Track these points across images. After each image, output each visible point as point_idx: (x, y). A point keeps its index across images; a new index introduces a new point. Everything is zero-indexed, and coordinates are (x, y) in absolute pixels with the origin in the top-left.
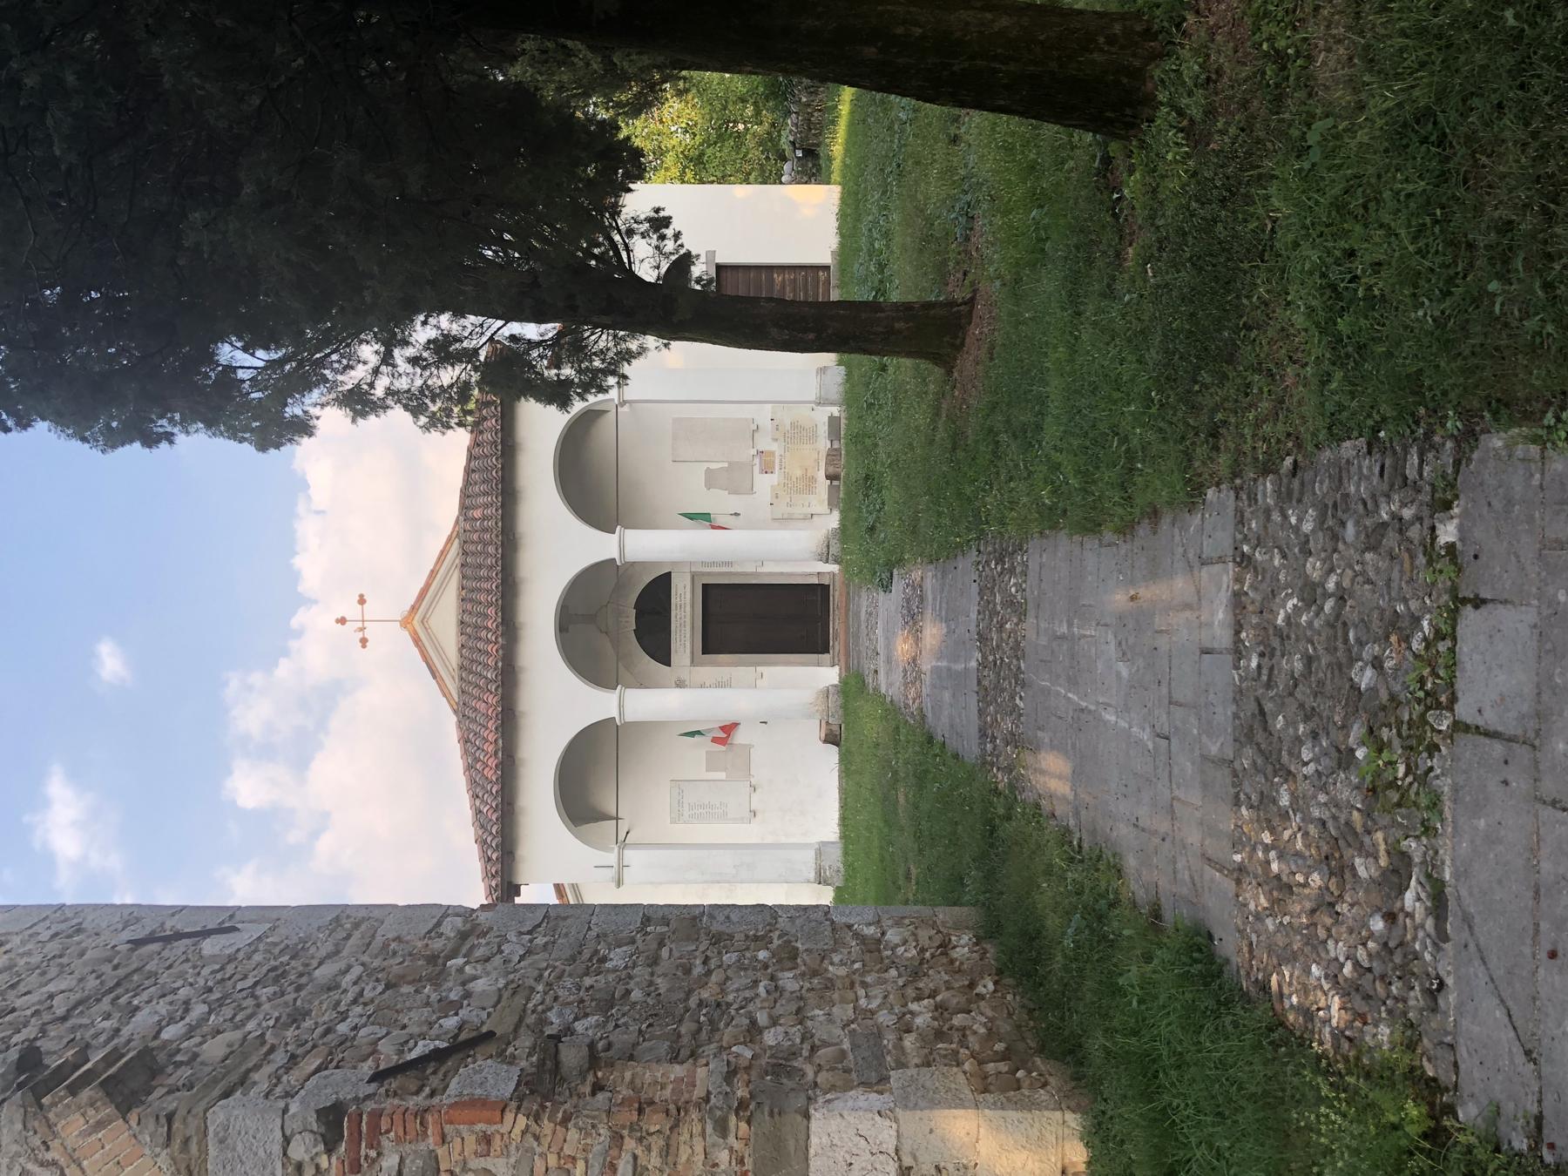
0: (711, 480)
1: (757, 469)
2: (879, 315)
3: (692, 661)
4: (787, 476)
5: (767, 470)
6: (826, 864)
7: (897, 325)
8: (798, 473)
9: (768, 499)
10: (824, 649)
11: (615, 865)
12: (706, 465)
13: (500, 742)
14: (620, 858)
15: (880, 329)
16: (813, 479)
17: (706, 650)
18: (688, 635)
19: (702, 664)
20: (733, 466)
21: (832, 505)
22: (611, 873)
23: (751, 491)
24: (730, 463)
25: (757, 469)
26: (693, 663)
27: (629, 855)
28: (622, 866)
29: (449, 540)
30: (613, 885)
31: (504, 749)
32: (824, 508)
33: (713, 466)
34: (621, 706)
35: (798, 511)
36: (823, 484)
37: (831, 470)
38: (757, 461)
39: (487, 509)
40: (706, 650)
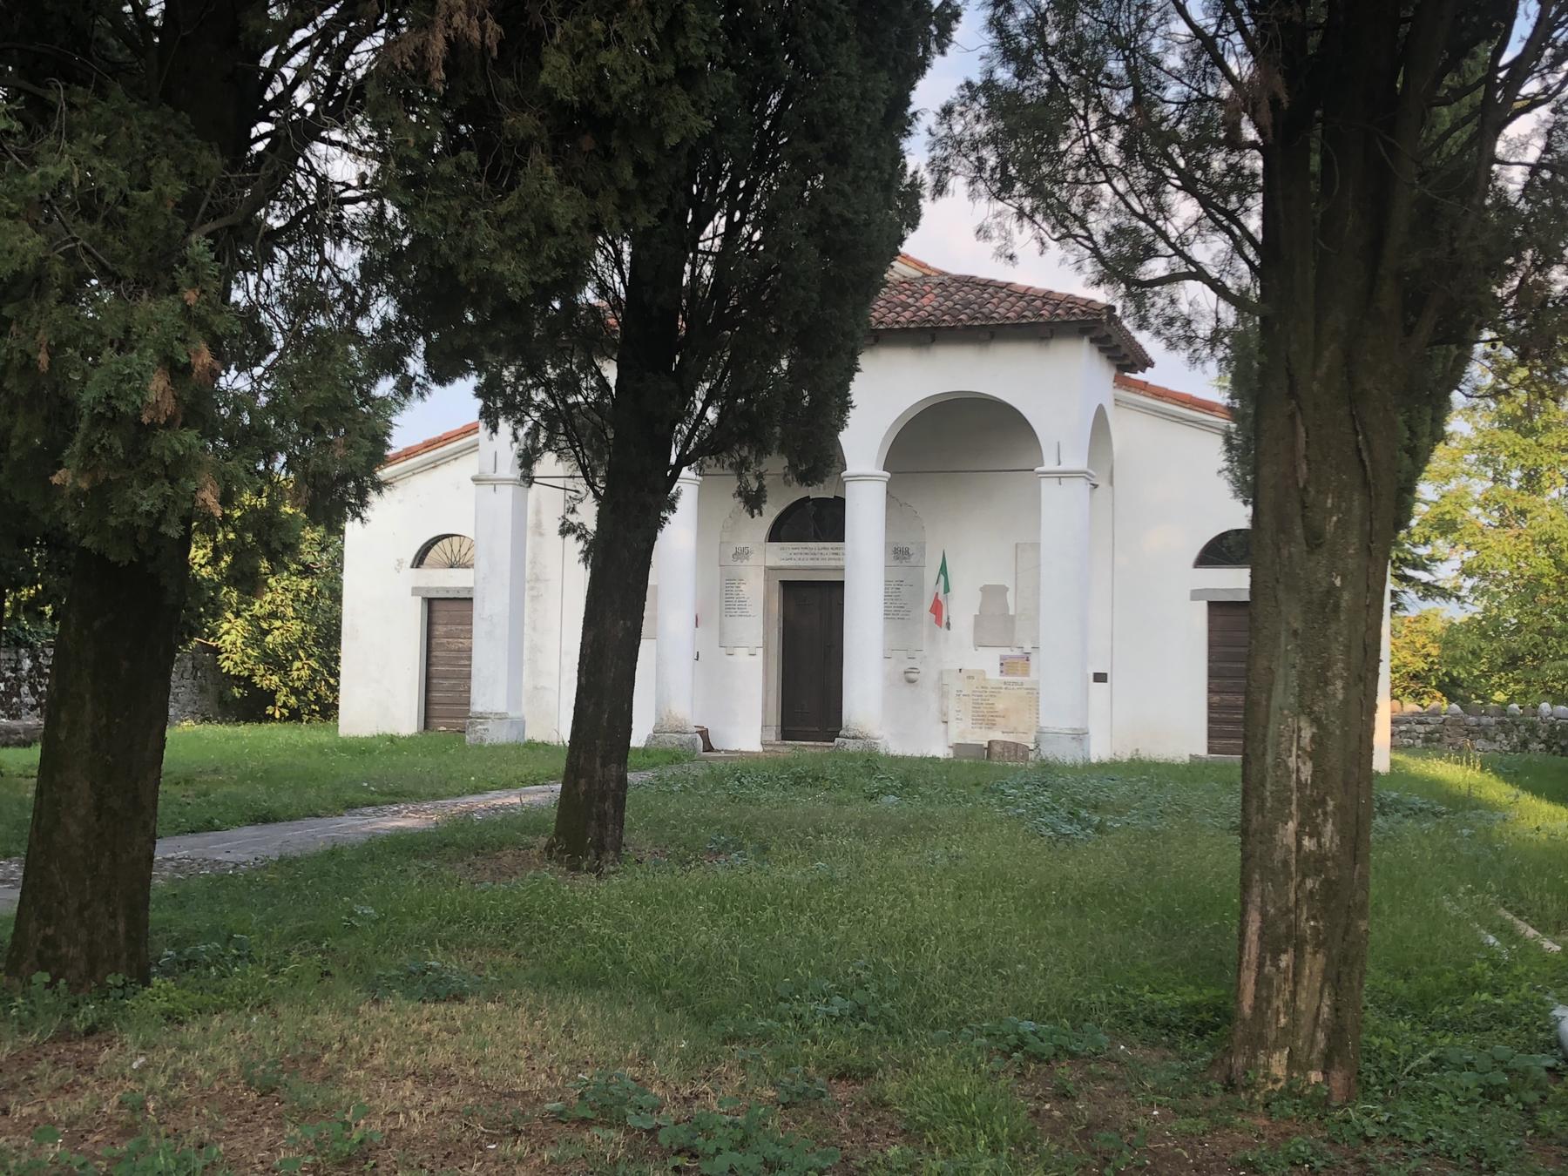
0: (992, 593)
1: (1007, 652)
2: (598, 761)
3: (772, 569)
4: (995, 691)
5: (1006, 666)
6: (490, 725)
7: (583, 781)
8: (1000, 706)
9: (969, 666)
10: (787, 733)
11: (496, 476)
12: (1010, 584)
13: (897, 326)
14: (504, 481)
15: (582, 761)
16: (991, 725)
17: (787, 586)
18: (801, 563)
19: (767, 580)
20: (1009, 621)
21: (958, 748)
22: (489, 472)
23: (979, 645)
24: (1013, 617)
25: (1007, 652)
26: (770, 570)
27: (507, 492)
28: (495, 483)
29: (920, 265)
30: (475, 473)
31: (890, 331)
32: (956, 739)
33: (1010, 597)
34: (1060, 476)
35: (952, 704)
36: (981, 737)
37: (997, 749)
38: (1017, 652)
39: (1003, 311)
40: (787, 586)
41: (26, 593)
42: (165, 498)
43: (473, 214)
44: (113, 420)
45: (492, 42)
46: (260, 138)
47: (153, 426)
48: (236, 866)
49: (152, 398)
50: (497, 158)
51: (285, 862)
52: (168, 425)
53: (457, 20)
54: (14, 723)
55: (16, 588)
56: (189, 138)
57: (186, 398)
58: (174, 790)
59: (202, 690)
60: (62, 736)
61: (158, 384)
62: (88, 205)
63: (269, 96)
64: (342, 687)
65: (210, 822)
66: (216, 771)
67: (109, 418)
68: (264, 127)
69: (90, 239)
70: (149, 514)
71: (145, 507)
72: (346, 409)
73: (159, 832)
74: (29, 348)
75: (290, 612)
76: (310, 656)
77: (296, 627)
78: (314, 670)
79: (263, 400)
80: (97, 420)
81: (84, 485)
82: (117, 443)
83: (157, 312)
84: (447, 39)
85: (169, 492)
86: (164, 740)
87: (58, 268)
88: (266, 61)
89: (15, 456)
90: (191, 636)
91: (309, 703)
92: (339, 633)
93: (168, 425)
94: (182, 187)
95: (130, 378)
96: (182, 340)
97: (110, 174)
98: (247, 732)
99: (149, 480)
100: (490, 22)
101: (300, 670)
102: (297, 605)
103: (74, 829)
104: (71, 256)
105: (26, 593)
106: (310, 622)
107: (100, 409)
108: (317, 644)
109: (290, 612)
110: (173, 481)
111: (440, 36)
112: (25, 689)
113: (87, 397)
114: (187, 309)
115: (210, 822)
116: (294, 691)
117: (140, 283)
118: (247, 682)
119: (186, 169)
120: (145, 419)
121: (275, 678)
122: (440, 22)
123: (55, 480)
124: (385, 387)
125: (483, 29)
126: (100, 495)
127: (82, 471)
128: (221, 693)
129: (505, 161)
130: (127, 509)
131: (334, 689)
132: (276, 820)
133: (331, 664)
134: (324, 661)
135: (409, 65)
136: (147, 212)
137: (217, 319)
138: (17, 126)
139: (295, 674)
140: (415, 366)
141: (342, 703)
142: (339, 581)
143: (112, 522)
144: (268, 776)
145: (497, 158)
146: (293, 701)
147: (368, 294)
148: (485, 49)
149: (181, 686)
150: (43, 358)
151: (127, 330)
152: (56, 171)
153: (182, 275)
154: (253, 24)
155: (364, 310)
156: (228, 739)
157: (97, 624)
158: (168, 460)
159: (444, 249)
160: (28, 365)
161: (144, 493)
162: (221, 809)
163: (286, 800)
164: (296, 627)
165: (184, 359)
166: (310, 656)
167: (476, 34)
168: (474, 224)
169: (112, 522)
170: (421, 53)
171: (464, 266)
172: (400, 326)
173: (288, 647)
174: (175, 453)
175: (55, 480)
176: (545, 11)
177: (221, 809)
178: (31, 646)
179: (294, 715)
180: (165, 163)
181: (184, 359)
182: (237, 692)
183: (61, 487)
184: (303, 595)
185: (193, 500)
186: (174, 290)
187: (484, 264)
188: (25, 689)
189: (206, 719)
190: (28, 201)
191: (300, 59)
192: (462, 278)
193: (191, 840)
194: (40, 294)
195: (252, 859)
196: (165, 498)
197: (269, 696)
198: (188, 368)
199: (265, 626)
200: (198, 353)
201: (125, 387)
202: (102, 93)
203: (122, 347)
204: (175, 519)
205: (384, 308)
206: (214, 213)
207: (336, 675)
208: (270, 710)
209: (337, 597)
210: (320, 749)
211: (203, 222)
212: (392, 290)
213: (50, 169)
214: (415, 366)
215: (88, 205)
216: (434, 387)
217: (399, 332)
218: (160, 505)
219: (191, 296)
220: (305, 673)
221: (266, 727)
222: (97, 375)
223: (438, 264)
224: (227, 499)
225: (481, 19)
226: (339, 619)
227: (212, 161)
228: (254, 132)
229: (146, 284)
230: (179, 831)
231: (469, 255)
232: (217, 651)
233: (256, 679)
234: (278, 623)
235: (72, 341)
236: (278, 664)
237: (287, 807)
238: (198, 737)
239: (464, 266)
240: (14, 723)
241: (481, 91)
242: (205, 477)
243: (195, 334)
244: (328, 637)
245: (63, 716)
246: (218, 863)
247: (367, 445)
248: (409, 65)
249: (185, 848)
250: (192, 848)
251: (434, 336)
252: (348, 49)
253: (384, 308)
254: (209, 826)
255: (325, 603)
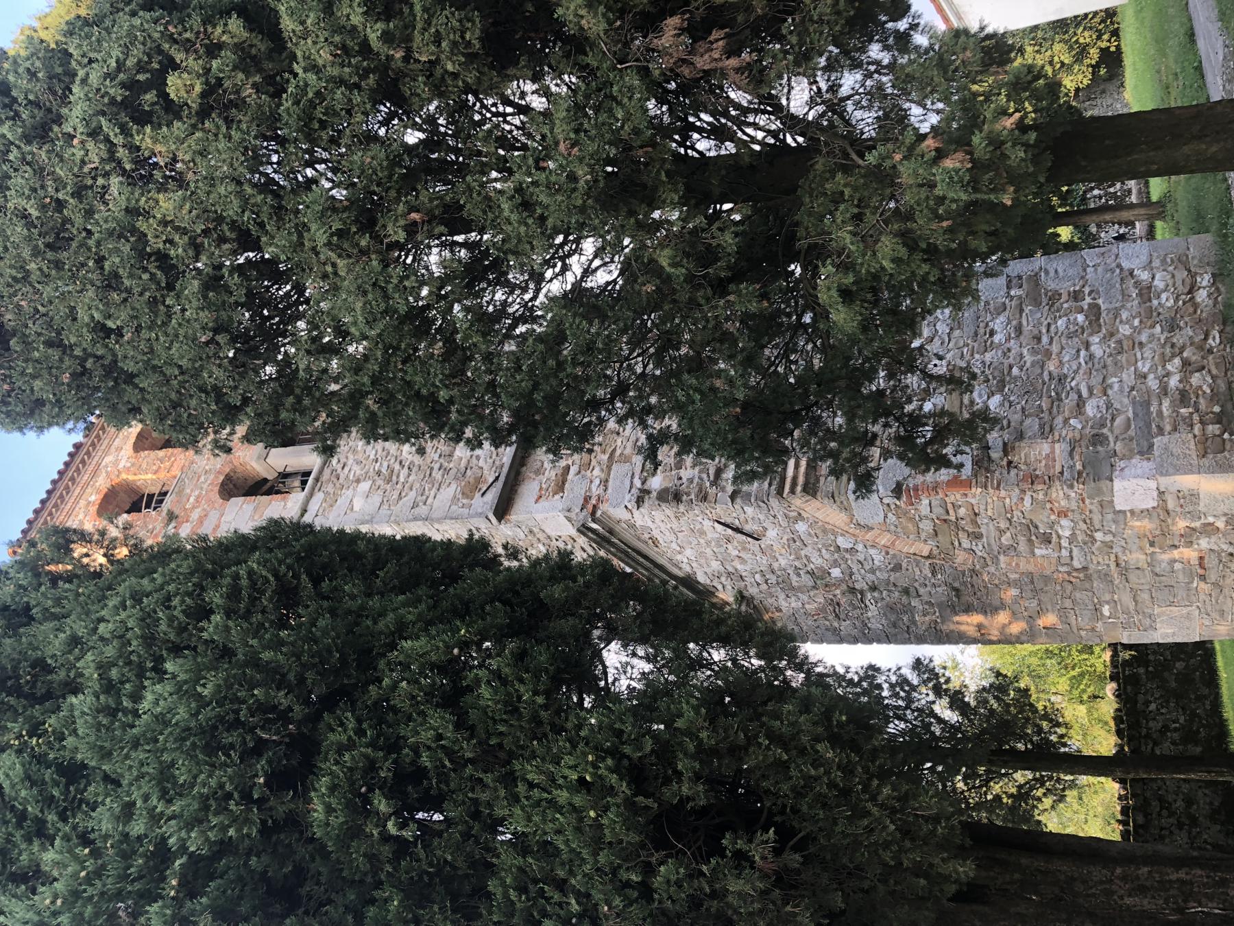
42: (1014, 146)
43: (816, 18)
45: (721, 33)
46: (795, 140)
47: (972, 161)
48: (1227, 46)
50: (779, 12)
52: (971, 153)
53: (717, 56)
54: (1134, 191)
55: (1052, 208)
56: (811, 177)
57: (954, 147)
58: (1174, 93)
59: (1103, 92)
61: (948, 163)
63: (772, 141)
64: (1094, 9)
65: (1196, 68)
66: (1158, 72)
67: (974, 184)
68: (789, 140)
69: (874, 214)
70: (1025, 152)
71: (1023, 155)
73: (1202, 100)
74: (941, 231)
77: (1057, 47)
78: (1085, 29)
79: (940, 105)
80: (976, 190)
82: (987, 176)
83: (906, 174)
84: (728, 58)
85: (1010, 144)
88: (757, 148)
89: (999, 225)
90: (1071, 107)
92: (1058, 21)
93: (971, 153)
94: (839, 176)
95: (951, 178)
96: (923, 156)
98: (1129, 60)
100: (712, 38)
101: (1085, 37)
102: (1043, 50)
103: (1214, 149)
104: (886, 222)
106: (1053, 41)
110: (1003, 143)
112: (1112, 190)
113: (964, 197)
114: (905, 158)
115: (1196, 68)
116: (1099, 38)
117: (893, 184)
119: (828, 175)
120: (970, 165)
121: (1092, 51)
122: (720, 65)
123: (1009, 203)
125: (717, 40)
126: (1016, 179)
129: (781, 7)
131: (1096, 13)
132: (1192, 28)
133: (1078, 20)
134: (1077, 25)
135: (746, 74)
136: (855, 189)
137: (907, 141)
138: (829, 261)
139: (1088, 40)
140: (902, 25)
142: (1024, 30)
144: (1160, 40)
146: (1106, 37)
147: (869, 63)
148: (727, 36)
150: (945, 224)
152: (848, 239)
153: (888, 163)
154: (747, 159)
155: (877, 63)
156: (1135, 69)
157: (1083, 163)
158: (991, 148)
160: (950, 230)
161: (1013, 157)
163: (1177, 26)
164: (1057, 47)
165: (933, 153)
166: (1075, 34)
167: (721, 43)
170: (738, 70)
171: (845, 14)
172: (883, 41)
175: (1009, 203)
176: (697, 9)
177: (1186, 64)
178: (1085, 192)
179: (1116, 33)
180: (827, 186)
181: (933, 153)
185: (1012, 130)
186: (894, 167)
188: (1112, 190)
189: (1122, 85)
190: (866, 247)
191: (750, 131)
192: (852, 13)
193: (1209, 78)
195: (1221, 38)
196: (1014, 146)
197: (1104, 52)
198: (937, 150)
199: (1058, 66)
200: (928, 146)
201: (956, 179)
202: (797, 224)
204: (1026, 137)
205: (875, 51)
206: (846, 155)
207: (1086, 15)
209: (1035, 28)
211: (852, 160)
212: (863, 50)
213: (848, 241)
214: (902, 25)
216: (913, 9)
217: (886, 39)
219: (898, 157)
220: (1086, 34)
221: (1124, 48)
225: (711, 43)
226: (1049, 24)
227: (820, 164)
228: (794, 145)
230: (1203, 86)
232: (1077, 90)
234: (1056, 59)
236: (1081, 53)
237: (1182, 24)
238: (1136, 87)
239: (845, 14)
240: (1134, 191)
241: (748, 32)
242: (998, 127)
243: (918, 150)
244: (1061, 26)
245: (1142, 169)
246: (1225, 58)
248: (746, 74)
250: (1215, 76)
251: (884, 19)
252: (737, 106)
253: (875, 51)
254: (1199, 69)
255: (1040, 34)
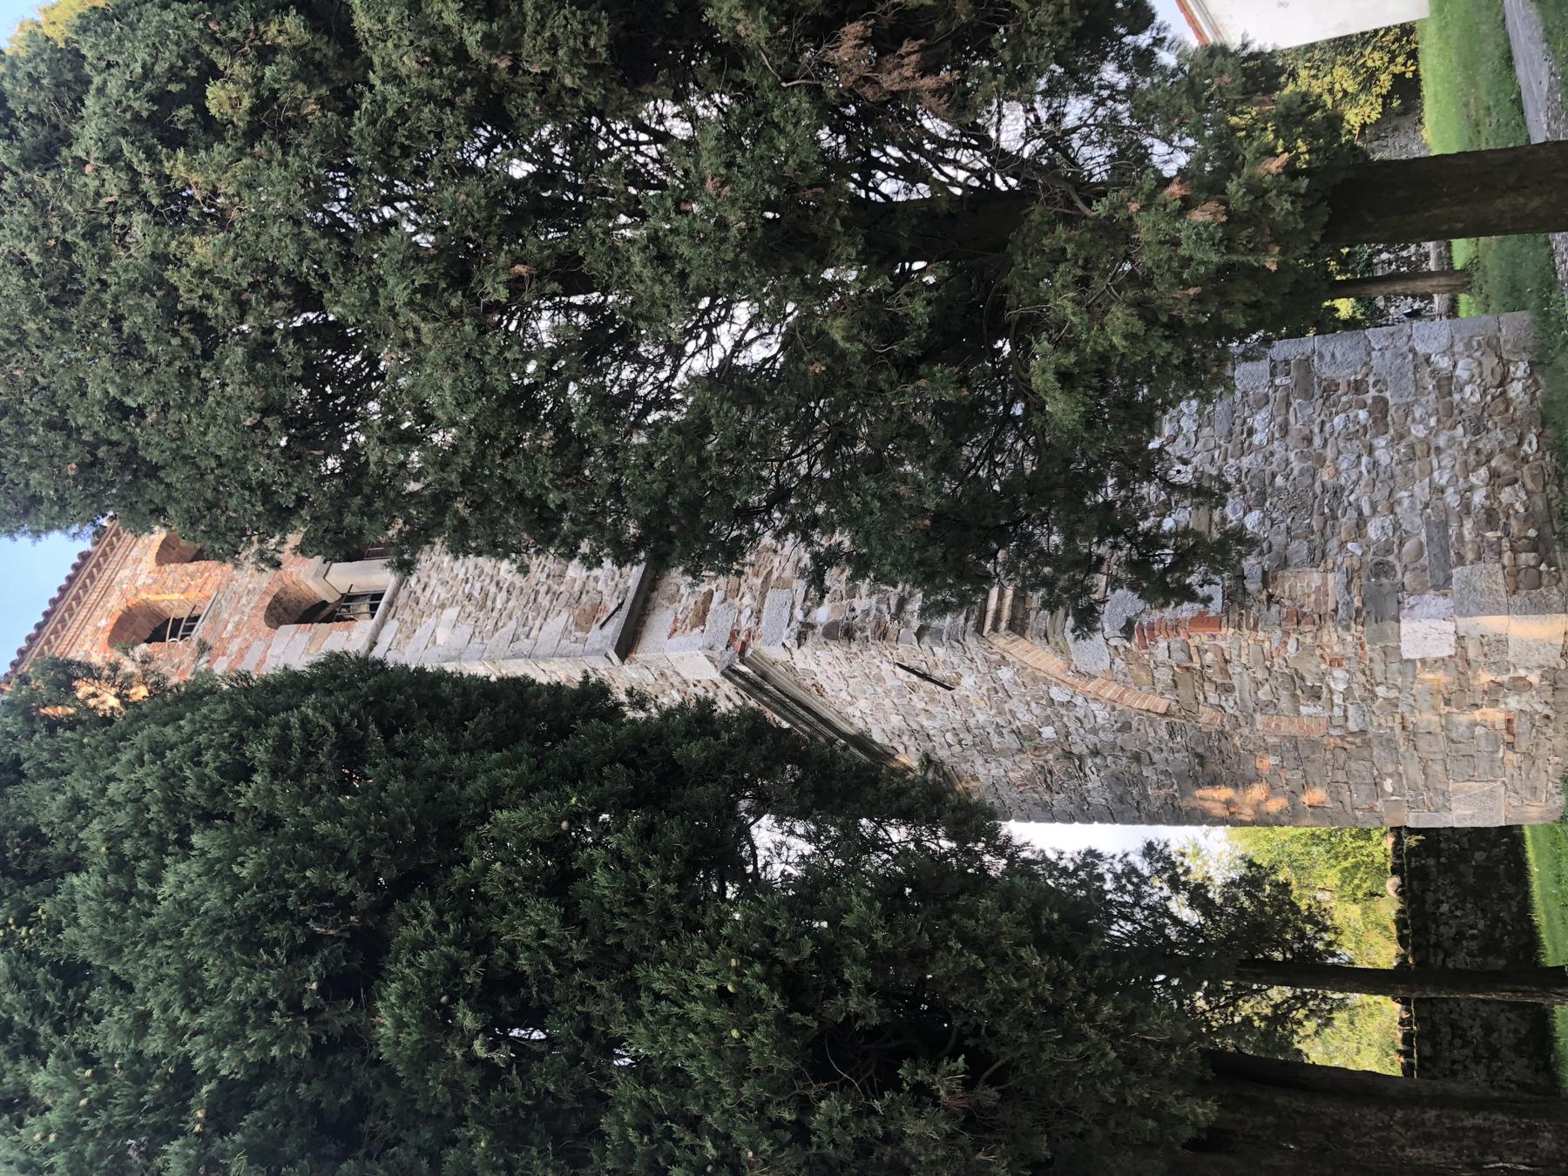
41: (1333, 265)
42: (1279, 195)
43: (1033, 28)
44: (1229, 239)
45: (915, 45)
46: (1005, 182)
47: (1228, 213)
49: (1209, 218)
51: (1549, 36)
52: (1226, 203)
53: (908, 74)
54: (1433, 256)
57: (1204, 196)
58: (1485, 132)
59: (1396, 129)
60: (1460, 225)
61: (1198, 216)
62: (1083, 282)
65: (1513, 101)
66: (1466, 105)
67: (1228, 243)
68: (999, 182)
70: (1293, 203)
71: (1288, 206)
72: (1192, 83)
74: (1187, 301)
75: (1328, 79)
76: (1362, 55)
77: (1339, 71)
78: (1374, 49)
79: (1190, 142)
80: (1230, 250)
81: (1277, 249)
82: (1245, 233)
84: (922, 77)
86: (1459, 154)
87: (1130, 294)
88: (958, 191)
89: (1261, 295)
91: (1402, 47)
92: (1340, 38)
93: (1226, 203)
94: (1060, 227)
96: (1165, 206)
97: (1065, 273)
99: (1267, 208)
100: (903, 51)
101: (1374, 59)
102: (1321, 75)
104: (1119, 288)
105: (1333, 265)
107: (1223, 249)
108: (1351, 52)
109: (1328, 79)
110: (1266, 191)
111: (922, 82)
113: (1215, 258)
114: (1143, 208)
116: (1392, 60)
117: (1128, 240)
118: (1386, 98)
119: (1046, 228)
120: (1224, 219)
121: (1382, 77)
124: (1167, 58)
125: (909, 54)
126: (1282, 237)
127: (1267, 252)
128: (1398, 115)
129: (991, 14)
130: (1291, 218)
131: (1388, 30)
132: (1509, 51)
133: (1365, 38)
134: (1365, 44)
136: (1080, 246)
138: (1044, 335)
139: (1378, 63)
141: (1399, 22)
142: (1297, 49)
143: (1301, 225)
144: (1469, 66)
145: (988, 19)
146: (1400, 60)
148: (922, 49)
149: (1387, 151)
150: (1192, 291)
151: (1161, 243)
153: (1120, 215)
154: (944, 206)
156: (1437, 101)
157: (1370, 219)
159: (1061, 42)
160: (1197, 299)
162: (1501, 95)
164: (1339, 71)
165: (1178, 203)
166: (1362, 55)
167: (914, 58)
168: (1040, 25)
169: (1301, 225)
170: (935, 92)
171: (1071, 25)
173: (1356, 73)
174: (1245, 194)
175: (1274, 268)
176: (885, 13)
177: (1501, 95)
178: (1371, 256)
179: (1413, 55)
180: (1045, 241)
181: (1178, 203)
182: (1396, 103)
183: (1278, 264)
184: (1313, 72)
185: (1279, 175)
186: (1130, 219)
187: (1067, 10)
188: (1404, 253)
192: (1080, 24)
194: (1148, 300)
196: (1279, 195)
197: (1398, 79)
198: (1183, 198)
199: (1340, 95)
200: (1172, 194)
203: (1176, 243)
204: (1295, 184)
206: (1070, 203)
207: (1376, 32)
208: (1409, 75)
210: (1442, 29)
211: (1077, 209)
212: (1094, 70)
213: (1069, 311)
214: (1144, 40)
215: (1083, 282)
216: (1158, 20)
218: (1285, 197)
219: (1134, 207)
220: (1376, 55)
222: (1199, 256)
223: (1073, 44)
224: (1271, 152)
225: (902, 57)
226: (1328, 42)
227: (1037, 213)
228: (1004, 188)
229: (1128, 237)
230: (1522, 125)
231: (1063, 23)
232: (1364, 126)
233: (1384, 91)
234: (1337, 86)
235: (1178, 275)
237: (1497, 46)
239: (1071, 25)
240: (1433, 256)
241: (948, 44)
242: (1260, 171)
243: (1160, 198)
244: (1344, 45)
245: (1444, 227)
246: (1550, 88)
247: (1219, 60)
249: (1537, 115)
250: (1537, 111)
252: (933, 138)
253: (1110, 72)
254: (1518, 103)
255: (1317, 54)
